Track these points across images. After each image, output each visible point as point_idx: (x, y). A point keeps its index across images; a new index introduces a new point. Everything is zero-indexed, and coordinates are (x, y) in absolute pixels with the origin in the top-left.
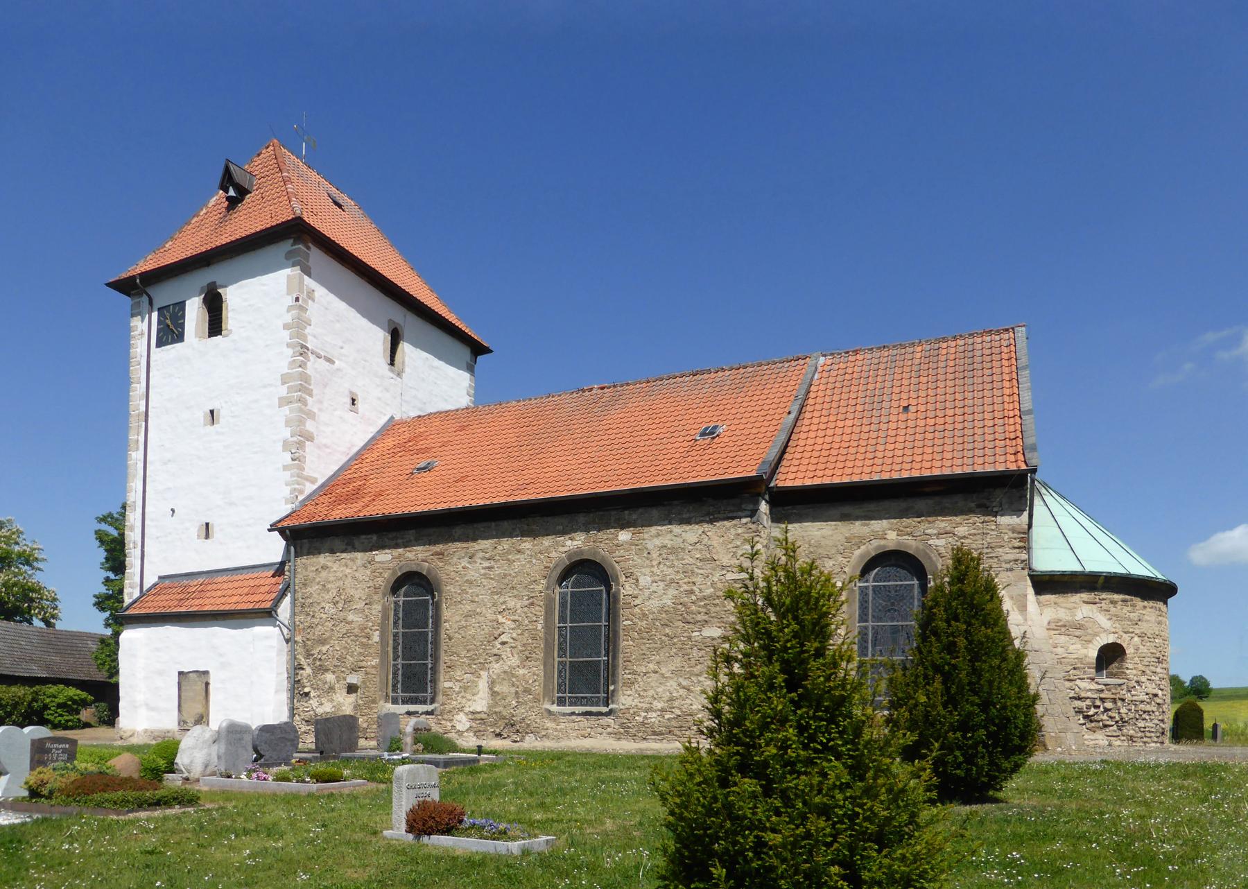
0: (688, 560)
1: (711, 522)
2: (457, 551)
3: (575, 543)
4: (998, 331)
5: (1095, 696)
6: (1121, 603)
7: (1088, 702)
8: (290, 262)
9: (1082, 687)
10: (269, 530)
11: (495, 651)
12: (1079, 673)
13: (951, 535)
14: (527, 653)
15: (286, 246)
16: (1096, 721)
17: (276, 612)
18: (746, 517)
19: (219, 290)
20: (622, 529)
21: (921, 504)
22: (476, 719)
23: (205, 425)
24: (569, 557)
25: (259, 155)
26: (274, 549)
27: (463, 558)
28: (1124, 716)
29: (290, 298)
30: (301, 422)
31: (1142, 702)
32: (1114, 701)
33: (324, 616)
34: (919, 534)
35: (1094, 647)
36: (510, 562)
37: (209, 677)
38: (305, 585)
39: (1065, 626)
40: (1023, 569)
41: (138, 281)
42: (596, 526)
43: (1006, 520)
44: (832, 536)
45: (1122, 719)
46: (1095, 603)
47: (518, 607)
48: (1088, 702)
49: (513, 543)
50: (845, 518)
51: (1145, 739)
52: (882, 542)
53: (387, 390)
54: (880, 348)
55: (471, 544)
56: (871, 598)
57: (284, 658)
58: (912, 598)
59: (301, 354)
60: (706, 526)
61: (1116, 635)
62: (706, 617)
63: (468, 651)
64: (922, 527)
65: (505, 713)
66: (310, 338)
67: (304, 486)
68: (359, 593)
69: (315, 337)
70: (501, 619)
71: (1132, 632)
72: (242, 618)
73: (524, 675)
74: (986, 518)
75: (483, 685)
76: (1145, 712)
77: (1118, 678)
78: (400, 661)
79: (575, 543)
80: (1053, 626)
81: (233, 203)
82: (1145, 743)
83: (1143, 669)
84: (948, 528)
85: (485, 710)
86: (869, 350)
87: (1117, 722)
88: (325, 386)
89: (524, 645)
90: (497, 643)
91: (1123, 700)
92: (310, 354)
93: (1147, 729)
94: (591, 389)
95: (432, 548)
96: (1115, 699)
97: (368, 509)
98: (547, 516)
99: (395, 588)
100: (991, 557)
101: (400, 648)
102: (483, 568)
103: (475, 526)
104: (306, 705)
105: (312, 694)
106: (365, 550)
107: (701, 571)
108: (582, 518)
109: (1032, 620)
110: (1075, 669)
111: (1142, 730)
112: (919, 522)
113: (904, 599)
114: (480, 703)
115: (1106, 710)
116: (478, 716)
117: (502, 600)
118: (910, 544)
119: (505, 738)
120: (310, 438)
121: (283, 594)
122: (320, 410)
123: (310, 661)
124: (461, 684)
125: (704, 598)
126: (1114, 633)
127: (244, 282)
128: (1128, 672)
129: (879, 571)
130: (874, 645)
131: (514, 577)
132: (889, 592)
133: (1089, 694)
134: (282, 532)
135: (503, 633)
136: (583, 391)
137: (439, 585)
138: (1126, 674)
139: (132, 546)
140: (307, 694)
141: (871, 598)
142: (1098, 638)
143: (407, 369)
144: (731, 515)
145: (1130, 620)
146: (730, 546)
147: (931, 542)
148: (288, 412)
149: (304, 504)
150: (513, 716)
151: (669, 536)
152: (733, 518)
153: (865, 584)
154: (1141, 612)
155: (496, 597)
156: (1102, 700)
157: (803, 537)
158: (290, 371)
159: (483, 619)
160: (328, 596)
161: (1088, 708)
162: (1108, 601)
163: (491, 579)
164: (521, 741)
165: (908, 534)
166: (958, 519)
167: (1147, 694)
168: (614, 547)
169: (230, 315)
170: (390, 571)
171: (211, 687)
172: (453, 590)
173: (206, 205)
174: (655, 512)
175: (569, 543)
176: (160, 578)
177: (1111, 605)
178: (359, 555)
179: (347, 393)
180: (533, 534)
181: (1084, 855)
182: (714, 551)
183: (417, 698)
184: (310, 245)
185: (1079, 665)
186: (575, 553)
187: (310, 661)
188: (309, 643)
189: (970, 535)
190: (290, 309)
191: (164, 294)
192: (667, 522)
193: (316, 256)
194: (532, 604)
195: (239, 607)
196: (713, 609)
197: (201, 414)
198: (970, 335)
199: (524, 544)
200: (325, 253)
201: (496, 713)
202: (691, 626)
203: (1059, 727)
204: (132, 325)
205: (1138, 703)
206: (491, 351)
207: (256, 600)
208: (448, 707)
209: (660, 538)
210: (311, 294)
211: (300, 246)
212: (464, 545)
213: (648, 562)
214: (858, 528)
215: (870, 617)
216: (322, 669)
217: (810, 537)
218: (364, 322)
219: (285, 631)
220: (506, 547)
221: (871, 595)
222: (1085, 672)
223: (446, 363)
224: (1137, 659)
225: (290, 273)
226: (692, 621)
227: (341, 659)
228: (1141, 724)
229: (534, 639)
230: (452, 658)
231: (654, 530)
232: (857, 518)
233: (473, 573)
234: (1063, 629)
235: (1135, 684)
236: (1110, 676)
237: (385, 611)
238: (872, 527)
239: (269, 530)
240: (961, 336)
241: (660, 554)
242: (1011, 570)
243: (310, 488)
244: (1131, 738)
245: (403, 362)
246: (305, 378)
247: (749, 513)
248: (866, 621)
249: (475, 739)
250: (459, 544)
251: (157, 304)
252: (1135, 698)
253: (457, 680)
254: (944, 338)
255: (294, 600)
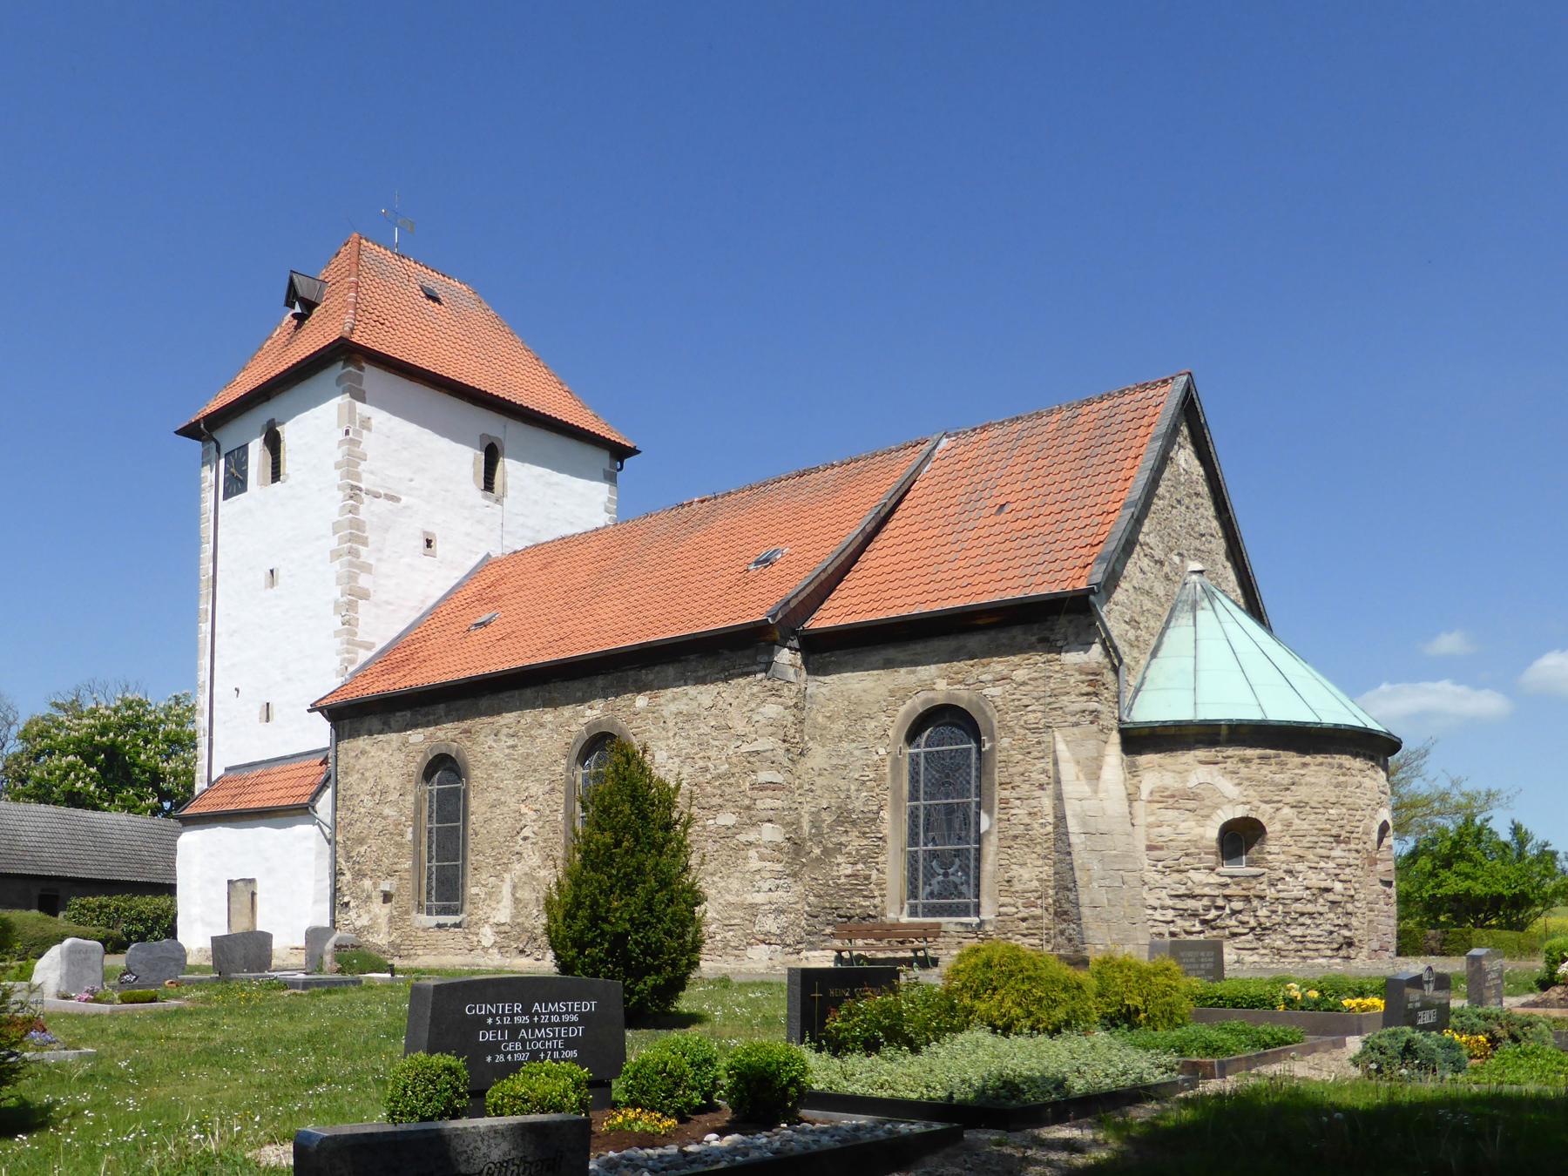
0: (704, 729)
1: (726, 680)
2: (481, 725)
3: (595, 712)
4: (1154, 384)
5: (1216, 893)
6: (1258, 761)
7: (1206, 901)
8: (340, 389)
9: (1196, 880)
10: (309, 711)
11: (517, 848)
12: (1192, 861)
13: (1009, 681)
14: (547, 850)
15: (338, 369)
16: (1219, 928)
17: (313, 808)
18: (761, 672)
19: (278, 429)
20: (639, 693)
21: (973, 641)
22: (501, 933)
23: (266, 587)
24: (588, 730)
25: (337, 255)
26: (320, 733)
27: (489, 735)
28: (1262, 920)
29: (340, 431)
30: (352, 577)
31: (1297, 900)
32: (1247, 899)
33: (362, 810)
34: (971, 681)
35: (1214, 824)
36: (533, 738)
37: (255, 886)
38: (346, 773)
39: (1173, 796)
40: (1092, 723)
41: (202, 426)
42: (613, 690)
43: (1072, 658)
44: (874, 689)
45: (1260, 924)
46: (1217, 763)
47: (540, 793)
48: (1206, 901)
49: (536, 716)
50: (888, 664)
51: (1305, 953)
52: (931, 695)
53: (479, 522)
54: (1013, 420)
55: (497, 718)
56: (922, 769)
57: (326, 862)
58: (969, 766)
59: (351, 497)
60: (721, 686)
61: (1248, 807)
62: (720, 801)
63: (493, 849)
64: (975, 671)
65: (526, 925)
66: (364, 476)
67: (357, 654)
68: (393, 782)
69: (372, 473)
70: (524, 810)
71: (1280, 801)
72: (285, 816)
73: (545, 877)
74: (1050, 656)
75: (506, 889)
76: (1302, 914)
77: (1259, 866)
78: (434, 862)
79: (593, 713)
80: (1157, 797)
81: (301, 319)
82: (1304, 958)
83: (1299, 852)
84: (1005, 672)
85: (508, 920)
86: (999, 424)
87: (1253, 929)
88: (387, 530)
89: (545, 841)
90: (519, 838)
91: (1262, 898)
92: (363, 495)
93: (1308, 939)
94: (691, 503)
95: (461, 724)
96: (1247, 897)
97: (377, 684)
98: (567, 680)
99: (428, 774)
100: (1055, 709)
101: (434, 846)
102: (508, 747)
103: (500, 696)
104: (346, 917)
105: (351, 905)
106: (399, 731)
107: (716, 743)
108: (600, 682)
109: (1106, 791)
110: (1187, 855)
111: (1298, 939)
112: (972, 666)
113: (960, 768)
114: (503, 914)
115: (1234, 912)
116: (502, 929)
117: (525, 785)
118: (962, 696)
119: (528, 955)
120: (364, 595)
121: (323, 786)
122: (379, 560)
123: (350, 864)
124: (486, 889)
125: (719, 777)
126: (1243, 803)
127: (298, 417)
128: (1269, 857)
129: (931, 732)
130: (926, 831)
131: (537, 757)
132: (943, 759)
133: (1207, 890)
134: (321, 710)
135: (525, 826)
136: (683, 506)
137: (466, 769)
138: (1267, 861)
139: (202, 733)
140: (347, 904)
141: (922, 769)
142: (1219, 812)
143: (510, 493)
144: (745, 670)
145: (1273, 783)
146: (745, 709)
147: (985, 692)
148: (339, 568)
149: (354, 675)
150: (535, 928)
151: (685, 700)
152: (748, 674)
153: (917, 750)
154: (1297, 771)
155: (519, 782)
156: (1227, 898)
157: (842, 692)
158: (340, 518)
159: (506, 809)
160: (366, 787)
161: (1207, 909)
162: (1235, 760)
163: (515, 760)
164: (543, 959)
165: (960, 683)
166: (1016, 659)
167: (1308, 888)
168: (632, 716)
169: (288, 456)
170: (422, 754)
171: (258, 898)
172: (479, 775)
173: (280, 324)
174: (671, 671)
175: (588, 712)
176: (226, 769)
177: (1240, 765)
178: (394, 736)
179: (419, 534)
180: (552, 703)
181: (703, 1089)
182: (729, 716)
183: (449, 907)
184: (364, 364)
185: (1193, 850)
186: (594, 724)
187: (350, 864)
188: (349, 843)
189: (1030, 679)
190: (341, 443)
191: (229, 437)
192: (682, 682)
193: (372, 376)
194: (553, 789)
195: (285, 802)
196: (728, 790)
197: (263, 575)
198: (1120, 392)
199: (545, 717)
200: (385, 370)
201: (518, 924)
202: (706, 812)
203: (1114, 937)
204: (202, 475)
205: (1288, 902)
206: (639, 452)
207: (298, 794)
208: (475, 918)
209: (676, 702)
210: (366, 424)
211: (350, 369)
212: (490, 720)
213: (664, 733)
214: (903, 677)
215: (922, 792)
216: (359, 875)
217: (850, 692)
218: (444, 443)
219: (327, 831)
220: (529, 720)
221: (922, 765)
222: (1200, 859)
223: (571, 475)
224: (1287, 838)
225: (341, 402)
226: (706, 806)
227: (378, 861)
228: (1299, 931)
229: (555, 832)
230: (478, 857)
231: (669, 692)
232: (903, 664)
233: (497, 753)
234: (1171, 801)
235: (1283, 875)
236: (1251, 863)
237: (418, 803)
238: (919, 676)
239: (309, 711)
240: (1109, 395)
241: (676, 723)
242: (1076, 724)
243: (364, 656)
244: (1279, 952)
245: (504, 485)
246: (357, 525)
247: (763, 666)
248: (917, 799)
249: (499, 957)
250: (486, 720)
251: (224, 450)
252: (1282, 895)
253: (483, 885)
254: (1088, 400)
255: (336, 793)
